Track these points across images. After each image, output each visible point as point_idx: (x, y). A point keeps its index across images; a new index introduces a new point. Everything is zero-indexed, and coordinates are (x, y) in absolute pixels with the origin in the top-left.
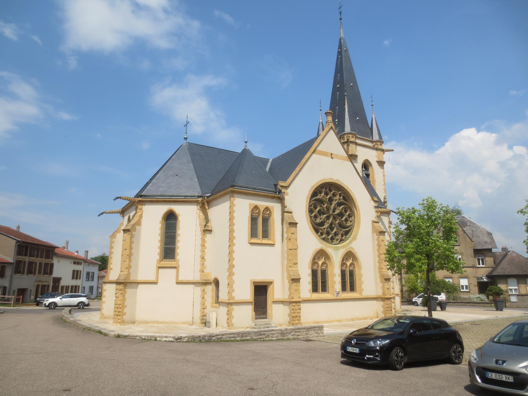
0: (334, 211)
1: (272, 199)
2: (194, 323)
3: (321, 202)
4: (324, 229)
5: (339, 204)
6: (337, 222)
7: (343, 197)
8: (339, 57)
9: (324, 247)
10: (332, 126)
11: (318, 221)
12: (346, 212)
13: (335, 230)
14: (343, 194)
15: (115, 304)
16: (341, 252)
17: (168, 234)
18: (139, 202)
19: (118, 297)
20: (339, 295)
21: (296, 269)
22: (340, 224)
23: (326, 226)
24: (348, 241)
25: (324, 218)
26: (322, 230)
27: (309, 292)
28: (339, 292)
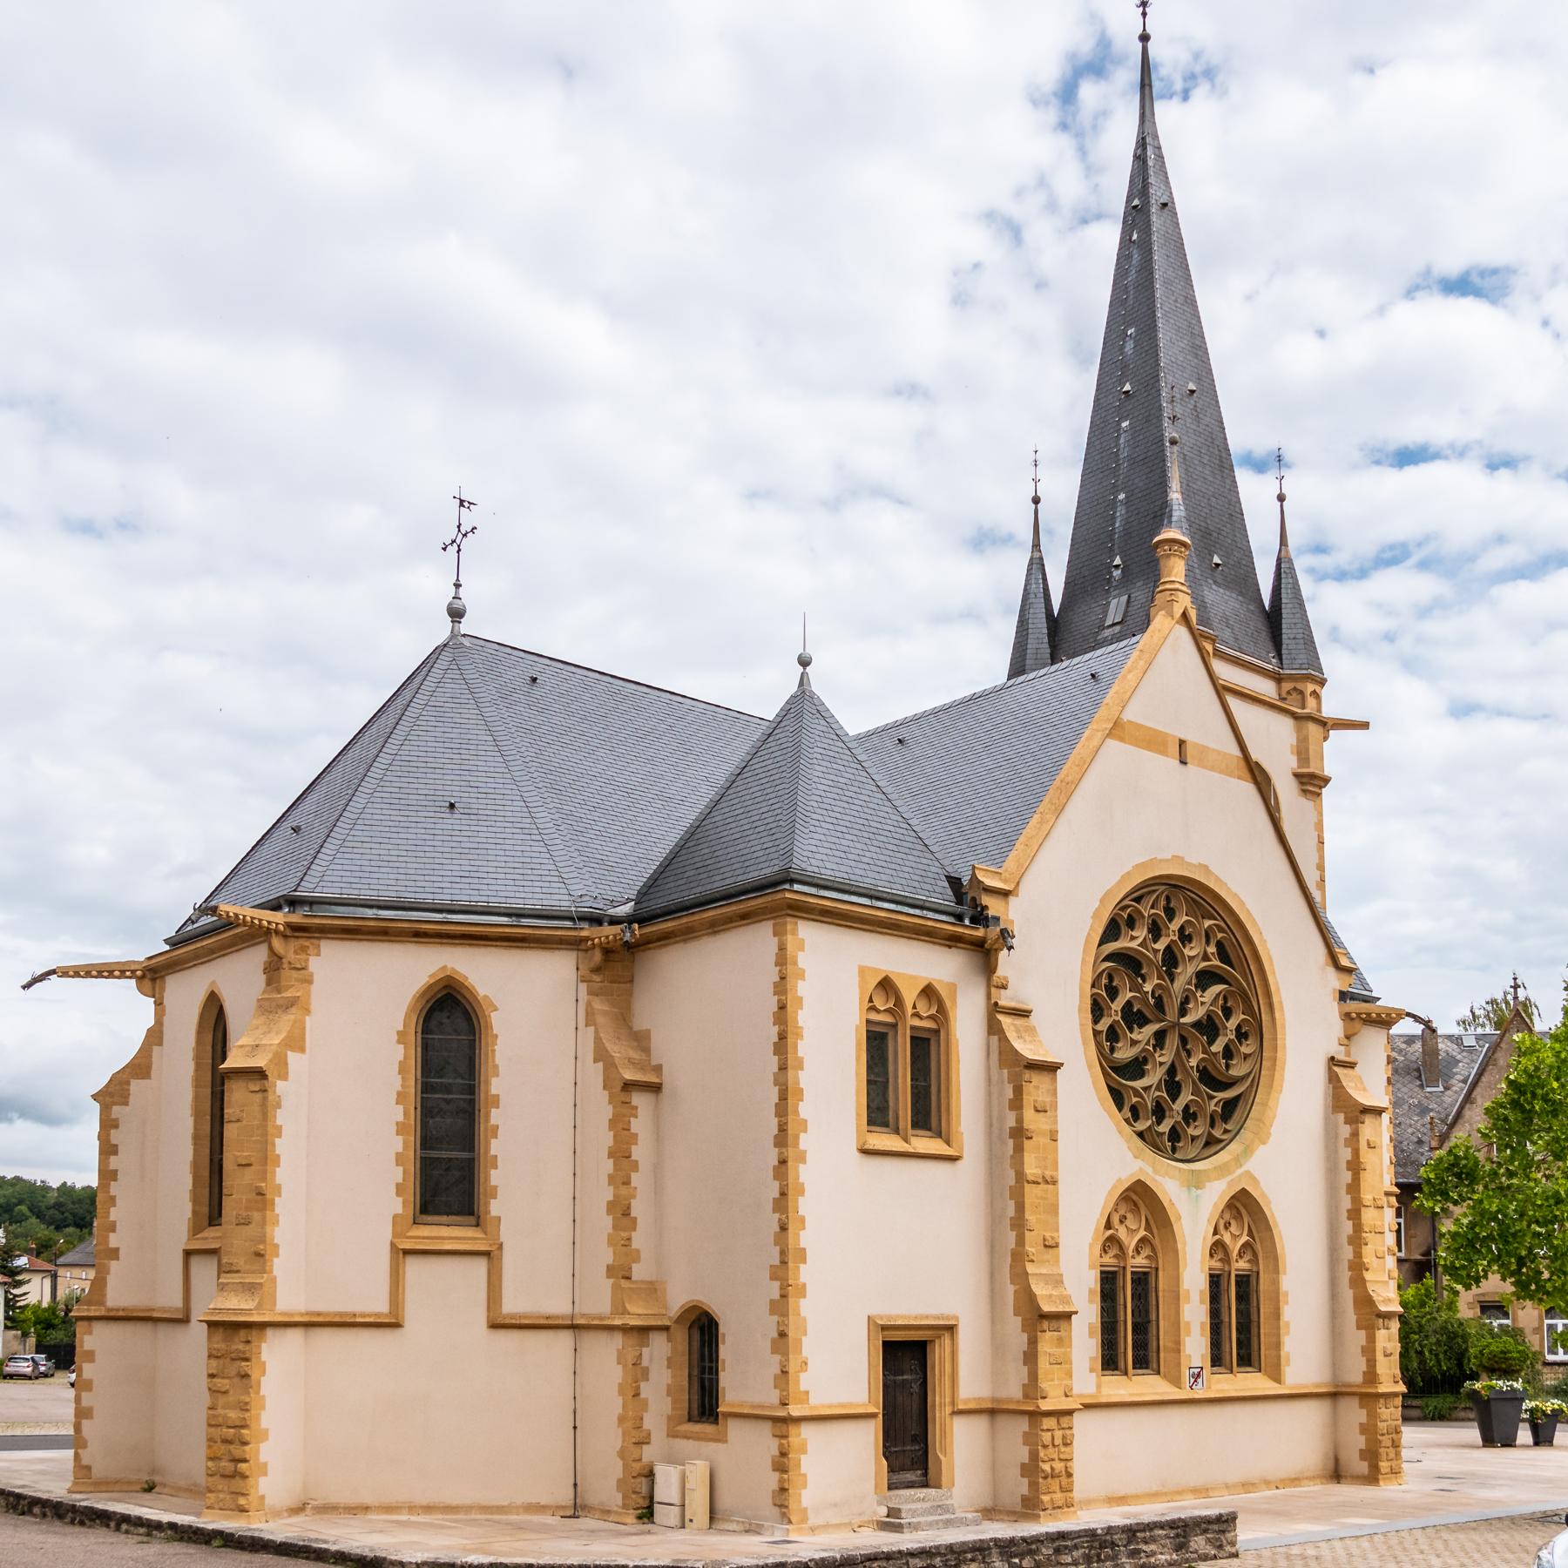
0: (1183, 1012)
1: (950, 947)
2: (584, 1507)
3: (1130, 962)
4: (1146, 1089)
5: (1205, 978)
6: (1193, 1062)
7: (1219, 945)
8: (1135, 237)
9: (1149, 1170)
10: (1186, 609)
11: (1124, 1053)
12: (1228, 1013)
13: (1186, 1097)
14: (1221, 930)
15: (210, 1425)
16: (1216, 1193)
17: (437, 1096)
18: (289, 933)
19: (223, 1390)
20: (1200, 1380)
21: (1055, 1271)
22: (1204, 1068)
23: (1154, 1077)
24: (1234, 1147)
25: (1148, 1043)
26: (1137, 1093)
27: (1092, 1370)
28: (1202, 1368)
